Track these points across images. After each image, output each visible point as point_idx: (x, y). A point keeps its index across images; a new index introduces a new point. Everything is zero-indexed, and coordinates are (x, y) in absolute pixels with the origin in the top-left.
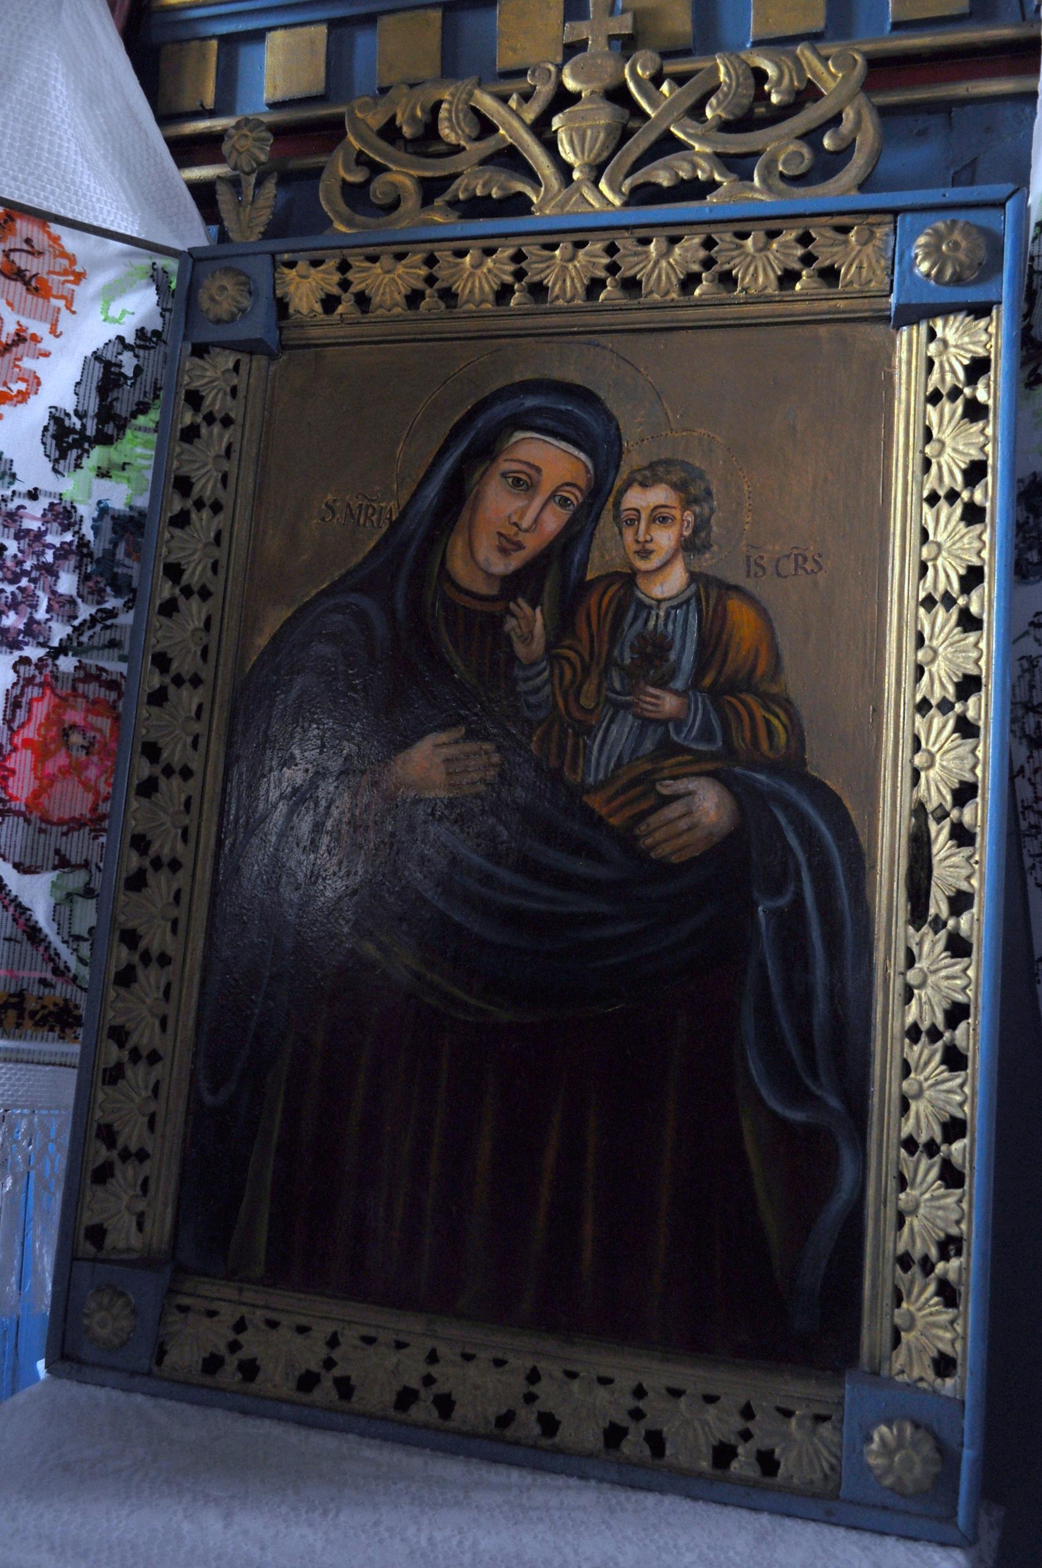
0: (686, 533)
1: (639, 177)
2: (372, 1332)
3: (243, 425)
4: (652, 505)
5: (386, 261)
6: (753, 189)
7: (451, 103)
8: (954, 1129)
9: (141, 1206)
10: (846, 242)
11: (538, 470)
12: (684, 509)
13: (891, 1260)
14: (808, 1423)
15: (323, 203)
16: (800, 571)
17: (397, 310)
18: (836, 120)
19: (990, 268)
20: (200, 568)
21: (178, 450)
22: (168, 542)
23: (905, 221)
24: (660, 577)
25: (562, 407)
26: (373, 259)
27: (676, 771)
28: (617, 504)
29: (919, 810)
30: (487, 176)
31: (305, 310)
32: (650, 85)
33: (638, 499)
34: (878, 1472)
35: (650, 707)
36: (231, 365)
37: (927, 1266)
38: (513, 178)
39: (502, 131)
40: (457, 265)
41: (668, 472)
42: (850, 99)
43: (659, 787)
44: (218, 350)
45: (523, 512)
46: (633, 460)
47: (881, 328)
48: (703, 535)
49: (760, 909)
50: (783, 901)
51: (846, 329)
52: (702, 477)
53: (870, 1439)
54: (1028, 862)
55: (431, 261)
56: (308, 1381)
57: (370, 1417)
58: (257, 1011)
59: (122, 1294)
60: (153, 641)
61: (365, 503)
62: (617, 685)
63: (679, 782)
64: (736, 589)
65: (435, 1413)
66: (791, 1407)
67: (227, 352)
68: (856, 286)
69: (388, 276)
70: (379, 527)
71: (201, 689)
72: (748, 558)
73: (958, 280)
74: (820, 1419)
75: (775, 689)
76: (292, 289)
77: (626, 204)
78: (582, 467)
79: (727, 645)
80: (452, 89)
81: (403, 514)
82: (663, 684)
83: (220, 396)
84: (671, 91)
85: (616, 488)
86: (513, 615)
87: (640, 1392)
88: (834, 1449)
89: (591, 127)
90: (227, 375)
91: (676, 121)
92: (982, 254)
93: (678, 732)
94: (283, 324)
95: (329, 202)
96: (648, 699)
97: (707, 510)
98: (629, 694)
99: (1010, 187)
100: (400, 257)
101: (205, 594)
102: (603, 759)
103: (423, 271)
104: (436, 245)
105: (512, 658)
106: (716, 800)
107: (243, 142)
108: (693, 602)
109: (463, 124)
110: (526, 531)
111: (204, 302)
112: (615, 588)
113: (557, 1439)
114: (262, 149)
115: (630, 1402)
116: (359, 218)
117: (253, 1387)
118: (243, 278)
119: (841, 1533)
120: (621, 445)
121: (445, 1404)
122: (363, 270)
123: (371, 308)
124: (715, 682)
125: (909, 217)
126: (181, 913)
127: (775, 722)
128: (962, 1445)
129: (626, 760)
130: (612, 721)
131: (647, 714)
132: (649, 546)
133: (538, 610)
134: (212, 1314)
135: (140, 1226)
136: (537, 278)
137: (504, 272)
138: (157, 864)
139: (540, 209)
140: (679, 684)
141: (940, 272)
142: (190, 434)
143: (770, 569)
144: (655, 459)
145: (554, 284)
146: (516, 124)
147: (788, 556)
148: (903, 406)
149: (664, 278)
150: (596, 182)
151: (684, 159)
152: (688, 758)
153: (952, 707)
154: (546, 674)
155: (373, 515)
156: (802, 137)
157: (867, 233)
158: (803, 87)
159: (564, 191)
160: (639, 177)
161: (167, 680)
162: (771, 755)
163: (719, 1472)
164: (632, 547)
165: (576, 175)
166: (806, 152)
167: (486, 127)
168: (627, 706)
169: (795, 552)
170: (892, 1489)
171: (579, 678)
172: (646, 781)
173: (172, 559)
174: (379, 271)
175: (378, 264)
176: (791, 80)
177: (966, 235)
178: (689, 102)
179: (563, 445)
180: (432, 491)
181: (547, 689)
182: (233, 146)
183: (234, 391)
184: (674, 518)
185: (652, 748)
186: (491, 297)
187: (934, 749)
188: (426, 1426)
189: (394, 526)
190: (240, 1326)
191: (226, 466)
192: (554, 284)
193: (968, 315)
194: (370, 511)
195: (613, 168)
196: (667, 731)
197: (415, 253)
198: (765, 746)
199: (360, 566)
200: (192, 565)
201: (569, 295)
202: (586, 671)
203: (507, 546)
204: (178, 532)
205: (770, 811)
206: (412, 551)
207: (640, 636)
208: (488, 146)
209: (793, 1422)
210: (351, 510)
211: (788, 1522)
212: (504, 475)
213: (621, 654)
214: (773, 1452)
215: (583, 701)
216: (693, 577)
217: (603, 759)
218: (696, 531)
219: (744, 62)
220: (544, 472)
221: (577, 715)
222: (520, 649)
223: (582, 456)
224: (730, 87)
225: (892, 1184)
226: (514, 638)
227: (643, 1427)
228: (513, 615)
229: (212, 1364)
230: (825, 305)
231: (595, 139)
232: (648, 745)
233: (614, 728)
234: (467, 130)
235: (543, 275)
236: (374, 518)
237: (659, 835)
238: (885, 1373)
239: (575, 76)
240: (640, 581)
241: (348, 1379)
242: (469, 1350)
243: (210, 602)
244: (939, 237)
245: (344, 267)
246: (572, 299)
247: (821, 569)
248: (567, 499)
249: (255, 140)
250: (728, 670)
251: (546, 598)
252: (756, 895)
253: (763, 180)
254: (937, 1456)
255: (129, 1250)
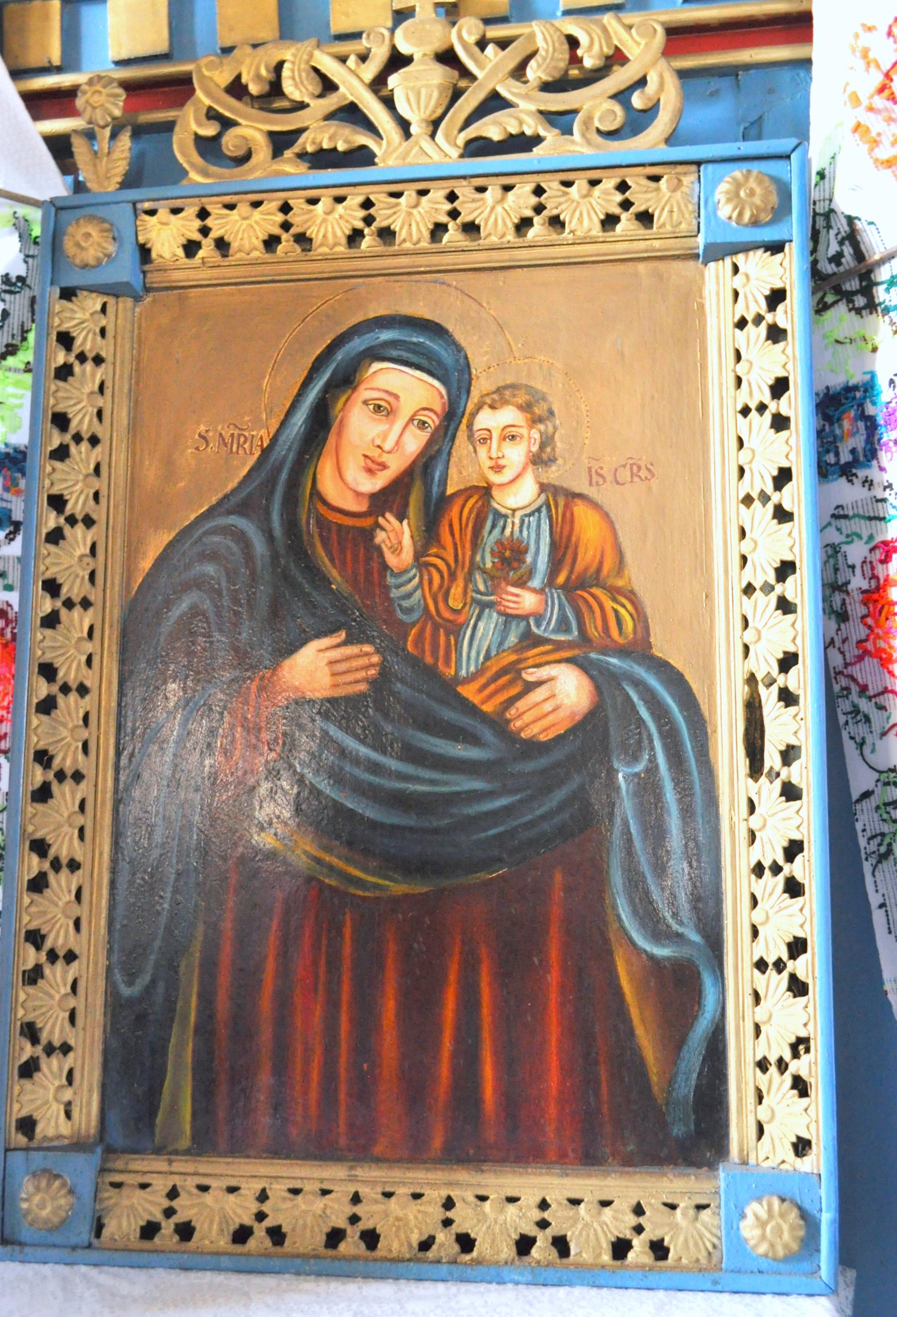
0: (535, 449)
1: (473, 131)
2: (297, 1185)
3: (114, 364)
4: (502, 426)
5: (243, 209)
6: (573, 142)
7: (293, 63)
8: (797, 947)
9: (68, 1095)
10: (658, 189)
11: (397, 397)
12: (531, 427)
13: (752, 1065)
14: (692, 1212)
15: (175, 147)
16: (636, 479)
17: (256, 254)
18: (642, 82)
19: (782, 211)
20: (82, 497)
21: (53, 388)
22: (50, 474)
23: (707, 170)
24: (513, 488)
25: (414, 340)
26: (231, 207)
27: (538, 660)
28: (470, 426)
29: (751, 680)
30: (332, 130)
31: (167, 255)
32: (476, 50)
33: (486, 420)
34: (752, 1242)
35: (512, 605)
36: (98, 307)
37: (782, 1065)
38: (357, 133)
39: (342, 89)
40: (311, 211)
41: (514, 396)
42: (654, 64)
43: (524, 675)
44: (85, 293)
45: (385, 438)
46: (481, 386)
47: (692, 264)
48: (549, 449)
49: (620, 775)
50: (639, 767)
51: (662, 266)
52: (544, 399)
53: (743, 1216)
54: (842, 719)
55: (286, 208)
56: (242, 1235)
57: (304, 1257)
58: (166, 906)
59: (57, 1176)
60: (42, 568)
61: (236, 432)
62: (482, 587)
63: (541, 669)
64: (580, 496)
65: (363, 1246)
66: (675, 1202)
67: (94, 295)
68: (669, 228)
69: (245, 223)
70: (251, 453)
71: (91, 611)
72: (590, 469)
73: (755, 223)
74: (700, 1207)
75: (620, 583)
76: (153, 235)
77: (462, 156)
78: (436, 393)
79: (576, 547)
80: (293, 50)
81: (274, 440)
82: (522, 583)
83: (90, 336)
84: (496, 55)
85: (468, 411)
86: (383, 529)
87: (544, 1205)
88: (714, 1231)
89: (426, 86)
90: (96, 317)
91: (502, 81)
92: (774, 199)
93: (538, 626)
94: (147, 267)
95: (184, 154)
96: (510, 598)
97: (551, 429)
98: (492, 595)
99: (794, 141)
100: (256, 204)
101: (89, 522)
102: (473, 653)
103: (280, 218)
104: (290, 194)
105: (385, 567)
106: (575, 683)
107: (96, 97)
108: (544, 510)
109: (305, 82)
110: (389, 452)
111: (68, 245)
112: (472, 501)
113: (475, 1254)
114: (116, 105)
115: (537, 1215)
116: (214, 169)
117: (192, 1244)
118: (106, 226)
119: (726, 1297)
120: (470, 373)
121: (371, 1238)
122: (222, 217)
123: (231, 251)
124: (568, 578)
125: (710, 167)
126: (86, 820)
127: (622, 611)
128: (821, 1210)
129: (493, 653)
130: (479, 618)
131: (509, 611)
132: (502, 462)
133: (405, 522)
134: (144, 1186)
135: (68, 1115)
136: (384, 224)
137: (355, 218)
138: (60, 776)
139: (384, 161)
140: (536, 583)
141: (741, 214)
142: (64, 372)
143: (609, 478)
144: (501, 384)
145: (401, 229)
146: (355, 82)
147: (624, 466)
148: (715, 333)
149: (500, 222)
150: (433, 136)
151: (511, 116)
152: (549, 647)
153: (773, 588)
154: (417, 580)
155: (245, 442)
156: (614, 97)
157: (675, 181)
158: (611, 52)
159: (405, 144)
160: (473, 131)
161: (59, 604)
162: (621, 641)
163: (619, 1263)
164: (487, 463)
165: (413, 129)
166: (618, 109)
167: (328, 86)
168: (490, 605)
169: (630, 462)
170: (766, 1256)
171: (446, 582)
172: (513, 670)
173: (55, 491)
174: (237, 217)
175: (235, 211)
176: (601, 48)
177: (760, 182)
178: (512, 64)
179: (418, 374)
180: (300, 418)
181: (418, 593)
182: (87, 102)
183: (103, 332)
184: (522, 437)
185: (516, 641)
186: (344, 241)
187: (760, 627)
188: (356, 1258)
189: (266, 452)
190: (173, 1194)
191: (100, 402)
192: (401, 229)
193: (766, 251)
194: (242, 439)
195: (447, 123)
196: (529, 625)
197: (271, 201)
198: (615, 632)
199: (235, 491)
200: (75, 496)
201: (415, 238)
202: (453, 576)
203: (373, 467)
204: (58, 465)
205: (623, 689)
206: (284, 475)
207: (499, 543)
208: (332, 102)
209: (678, 1211)
210: (223, 440)
211: (680, 1294)
212: (365, 402)
213: (483, 558)
214: (662, 1240)
215: (451, 603)
216: (543, 488)
217: (473, 653)
218: (542, 446)
219: (558, 29)
220: (402, 399)
221: (447, 615)
222: (391, 560)
223: (436, 383)
224: (547, 51)
225: (749, 1000)
226: (385, 549)
227: (549, 1232)
228: (383, 529)
229: (150, 1230)
230: (643, 245)
231: (430, 97)
232: (512, 639)
233: (481, 625)
234: (310, 88)
235: (390, 221)
236: (246, 446)
237: (527, 718)
238: (752, 1161)
239: (406, 37)
240: (495, 492)
241: (279, 1227)
242: (388, 1189)
243: (94, 529)
244: (738, 185)
245: (203, 214)
246: (418, 242)
247: (653, 475)
248: (424, 423)
249: (109, 95)
250: (579, 566)
251: (412, 510)
252: (616, 765)
253: (583, 135)
254: (802, 1222)
255: (60, 1137)
